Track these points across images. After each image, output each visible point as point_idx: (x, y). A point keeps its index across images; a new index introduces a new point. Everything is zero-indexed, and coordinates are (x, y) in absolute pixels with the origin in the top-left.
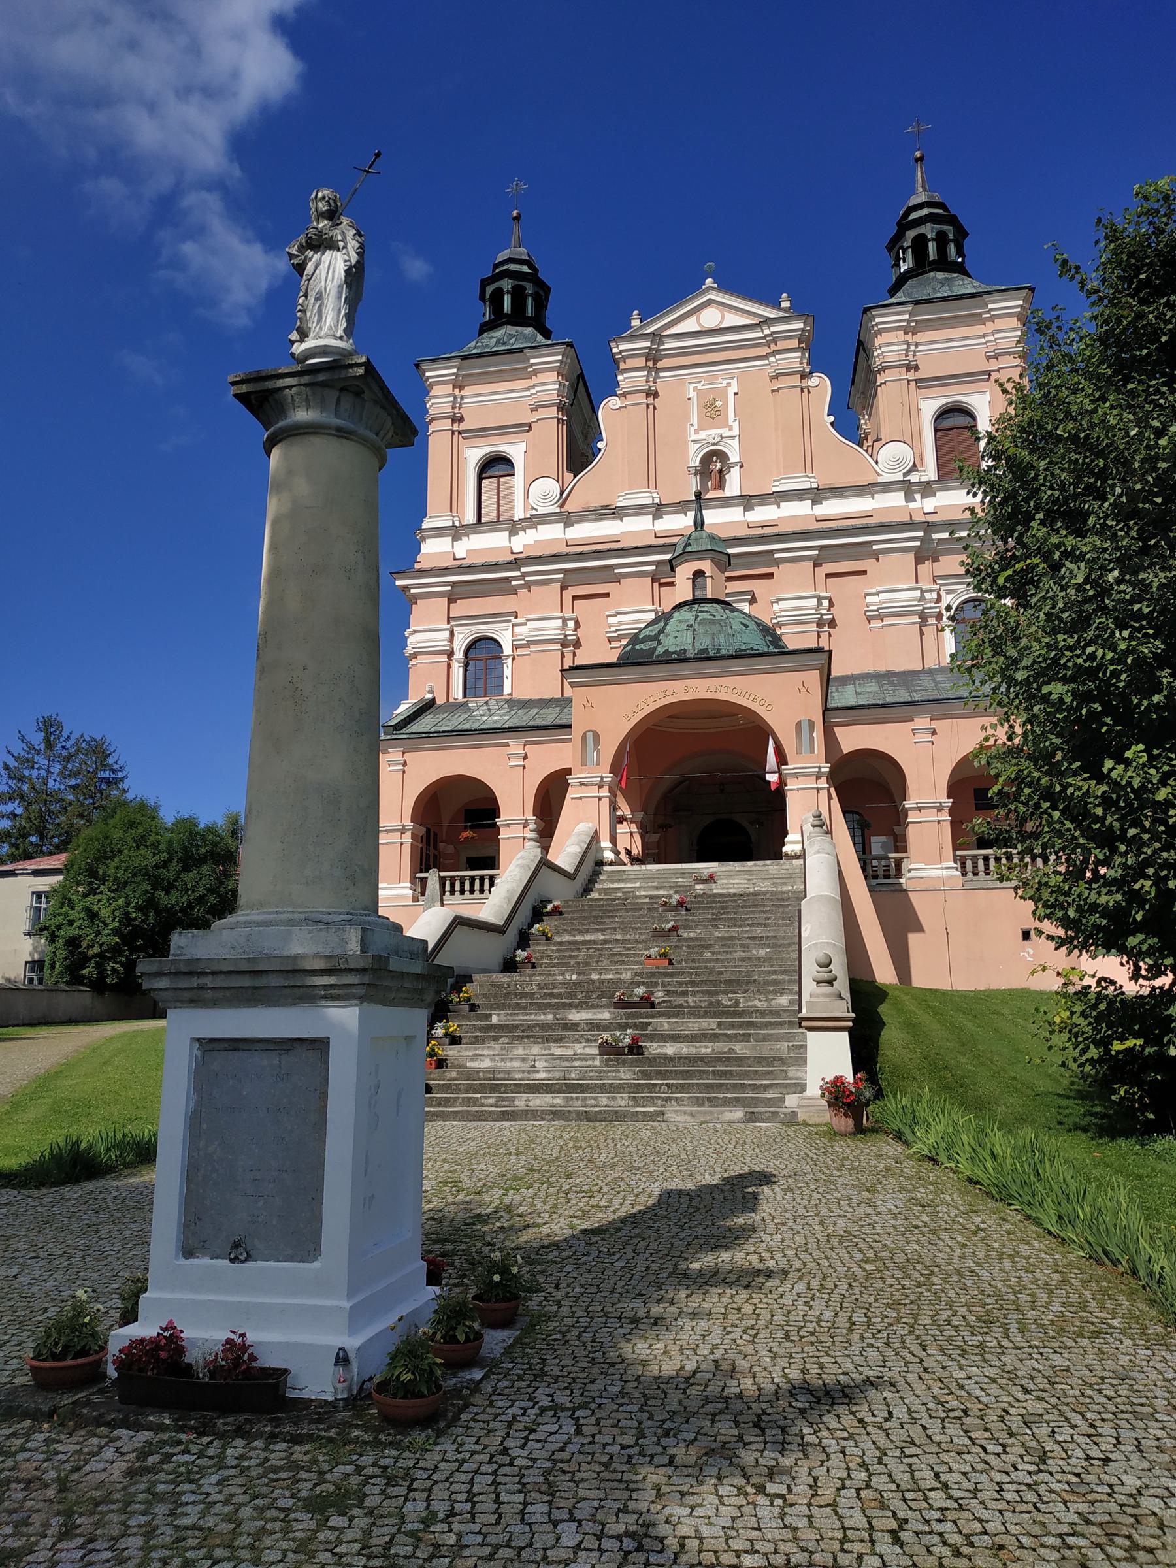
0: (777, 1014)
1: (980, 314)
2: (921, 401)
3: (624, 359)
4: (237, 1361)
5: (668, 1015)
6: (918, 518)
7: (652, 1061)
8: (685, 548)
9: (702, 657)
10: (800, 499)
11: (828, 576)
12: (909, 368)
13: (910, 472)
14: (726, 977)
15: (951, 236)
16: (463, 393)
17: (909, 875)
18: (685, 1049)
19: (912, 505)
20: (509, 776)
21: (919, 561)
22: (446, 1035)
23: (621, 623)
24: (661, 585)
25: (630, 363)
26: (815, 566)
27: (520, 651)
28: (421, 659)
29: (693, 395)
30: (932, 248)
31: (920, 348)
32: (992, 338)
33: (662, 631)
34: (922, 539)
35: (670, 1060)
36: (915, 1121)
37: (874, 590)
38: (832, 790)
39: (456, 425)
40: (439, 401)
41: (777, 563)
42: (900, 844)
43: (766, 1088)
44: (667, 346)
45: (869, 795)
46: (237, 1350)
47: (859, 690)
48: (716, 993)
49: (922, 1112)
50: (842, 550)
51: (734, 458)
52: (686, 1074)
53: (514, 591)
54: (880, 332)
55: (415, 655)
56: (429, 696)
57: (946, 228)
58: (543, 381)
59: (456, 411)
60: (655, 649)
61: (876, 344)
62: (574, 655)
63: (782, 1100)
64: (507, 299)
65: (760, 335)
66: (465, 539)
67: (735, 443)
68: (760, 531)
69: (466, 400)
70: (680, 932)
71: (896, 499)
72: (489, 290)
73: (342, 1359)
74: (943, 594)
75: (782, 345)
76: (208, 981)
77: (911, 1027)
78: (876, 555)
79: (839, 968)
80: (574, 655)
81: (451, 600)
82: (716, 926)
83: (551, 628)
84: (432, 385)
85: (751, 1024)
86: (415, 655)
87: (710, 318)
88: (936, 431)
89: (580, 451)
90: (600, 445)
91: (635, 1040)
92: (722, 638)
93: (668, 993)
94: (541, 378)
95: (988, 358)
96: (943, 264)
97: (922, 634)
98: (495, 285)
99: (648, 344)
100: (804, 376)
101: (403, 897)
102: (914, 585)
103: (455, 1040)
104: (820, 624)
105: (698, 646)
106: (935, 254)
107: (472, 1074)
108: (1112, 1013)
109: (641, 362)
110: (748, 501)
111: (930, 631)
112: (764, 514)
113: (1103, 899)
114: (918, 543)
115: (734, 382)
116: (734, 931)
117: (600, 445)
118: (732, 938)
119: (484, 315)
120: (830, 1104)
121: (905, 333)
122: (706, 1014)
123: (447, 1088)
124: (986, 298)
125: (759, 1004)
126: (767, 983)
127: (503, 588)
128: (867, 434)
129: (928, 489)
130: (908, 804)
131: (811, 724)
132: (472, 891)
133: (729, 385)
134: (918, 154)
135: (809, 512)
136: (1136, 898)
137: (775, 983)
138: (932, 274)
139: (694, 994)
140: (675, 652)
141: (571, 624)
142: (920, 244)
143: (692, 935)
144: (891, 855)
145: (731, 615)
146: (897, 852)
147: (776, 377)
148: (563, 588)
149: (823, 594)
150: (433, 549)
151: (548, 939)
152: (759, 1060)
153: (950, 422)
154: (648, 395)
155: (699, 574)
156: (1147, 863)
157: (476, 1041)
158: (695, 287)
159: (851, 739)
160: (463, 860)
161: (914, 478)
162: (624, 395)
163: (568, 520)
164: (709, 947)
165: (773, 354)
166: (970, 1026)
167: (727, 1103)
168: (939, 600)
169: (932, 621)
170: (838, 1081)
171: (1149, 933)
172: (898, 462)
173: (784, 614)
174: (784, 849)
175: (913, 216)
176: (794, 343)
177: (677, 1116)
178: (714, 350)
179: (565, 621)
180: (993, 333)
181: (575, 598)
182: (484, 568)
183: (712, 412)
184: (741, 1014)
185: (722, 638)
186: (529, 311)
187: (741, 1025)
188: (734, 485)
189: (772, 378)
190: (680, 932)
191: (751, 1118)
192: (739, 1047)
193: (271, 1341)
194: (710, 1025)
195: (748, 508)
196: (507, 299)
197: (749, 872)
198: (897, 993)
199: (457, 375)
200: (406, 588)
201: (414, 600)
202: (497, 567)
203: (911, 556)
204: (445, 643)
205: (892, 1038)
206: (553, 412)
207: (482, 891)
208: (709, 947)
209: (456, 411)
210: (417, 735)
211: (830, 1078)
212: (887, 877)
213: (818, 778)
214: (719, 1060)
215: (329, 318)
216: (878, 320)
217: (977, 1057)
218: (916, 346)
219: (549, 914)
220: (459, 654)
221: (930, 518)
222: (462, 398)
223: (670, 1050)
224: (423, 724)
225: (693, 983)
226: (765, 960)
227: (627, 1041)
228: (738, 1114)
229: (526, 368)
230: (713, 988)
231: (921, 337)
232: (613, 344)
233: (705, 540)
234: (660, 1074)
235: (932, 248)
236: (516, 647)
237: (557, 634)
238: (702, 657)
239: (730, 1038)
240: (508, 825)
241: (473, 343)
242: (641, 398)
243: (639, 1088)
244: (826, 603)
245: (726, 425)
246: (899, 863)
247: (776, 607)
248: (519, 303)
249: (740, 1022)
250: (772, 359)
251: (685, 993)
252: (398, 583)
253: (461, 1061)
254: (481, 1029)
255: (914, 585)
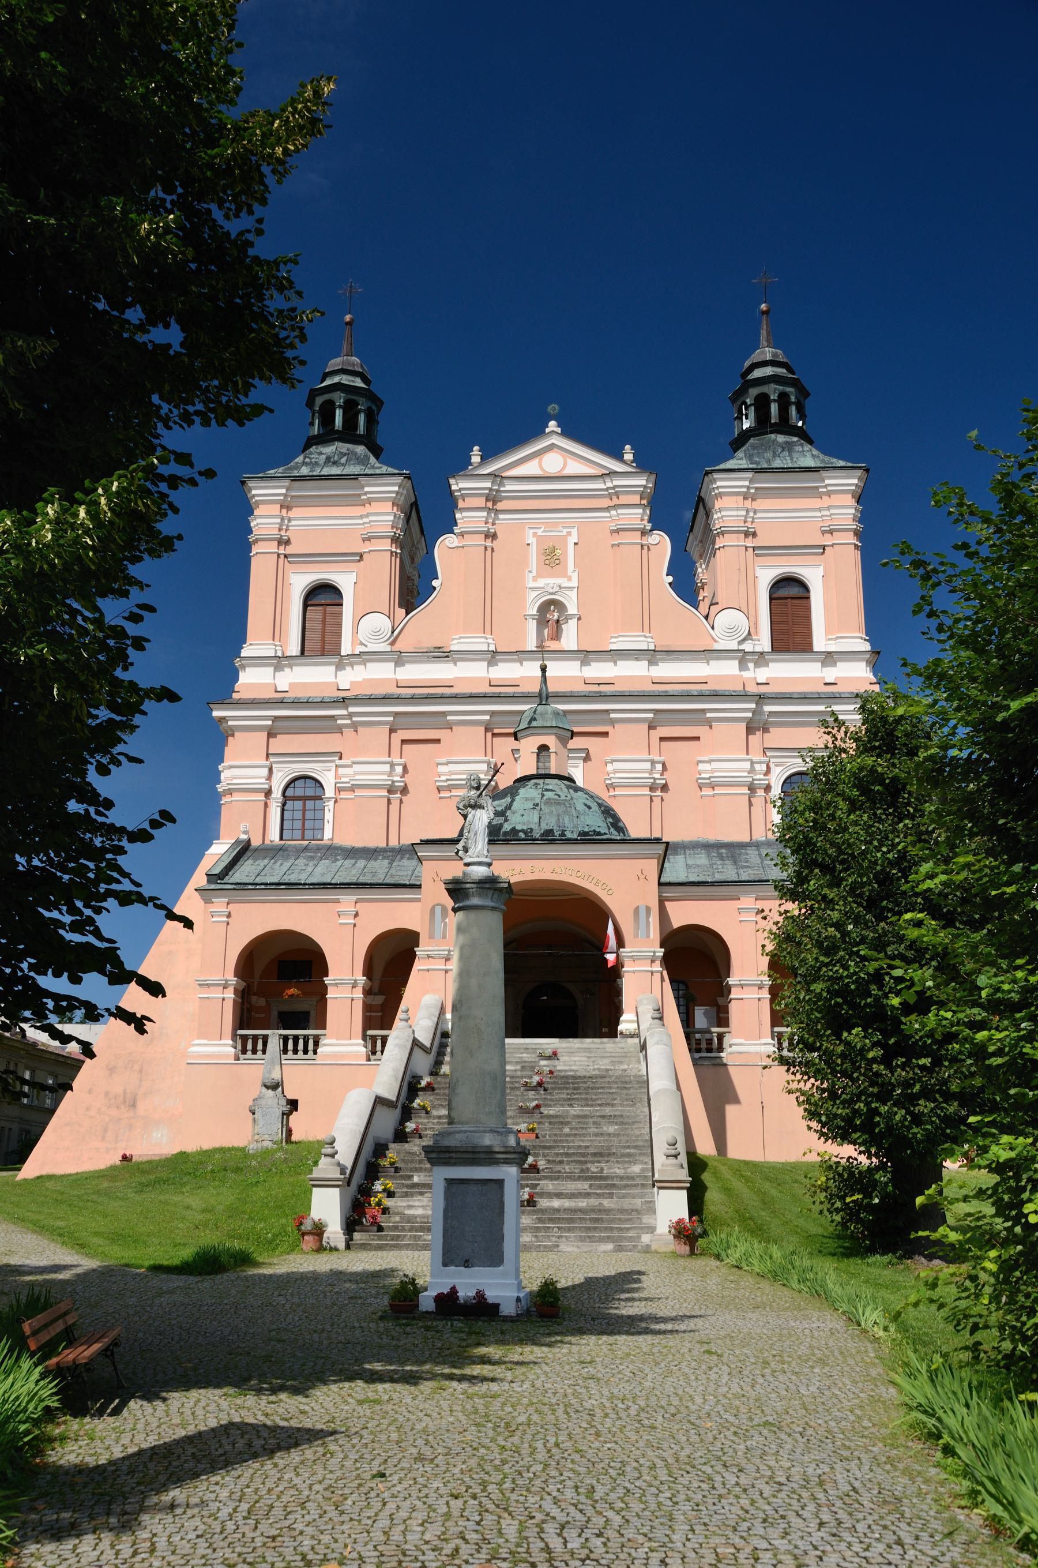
0: (632, 1178)
1: (817, 488)
2: (757, 569)
3: (463, 497)
4: (479, 1302)
5: (551, 1179)
6: (752, 689)
7: (543, 1211)
8: (530, 722)
9: (548, 838)
10: (637, 659)
11: (662, 739)
12: (747, 534)
13: (744, 640)
14: (592, 1151)
15: (793, 399)
16: (291, 514)
17: (729, 1050)
18: (567, 1203)
19: (746, 674)
20: (343, 934)
21: (750, 730)
22: (384, 1190)
23: (451, 773)
24: (494, 735)
25: (469, 502)
26: (650, 728)
27: (343, 795)
28: (237, 797)
29: (532, 540)
30: (774, 408)
31: (759, 515)
32: (827, 513)
33: (509, 807)
34: (754, 712)
35: (558, 1210)
36: (728, 1247)
37: (706, 758)
38: (665, 973)
39: (282, 548)
40: (264, 522)
41: (613, 722)
42: (722, 1018)
43: (628, 1229)
44: (508, 488)
45: (696, 965)
46: (480, 1295)
47: (690, 862)
48: (586, 1162)
49: (733, 1240)
50: (679, 714)
51: (572, 609)
52: (571, 1220)
53: (339, 730)
54: (720, 495)
55: (230, 792)
56: (244, 837)
57: (788, 389)
58: (376, 508)
59: (283, 533)
60: (501, 825)
61: (717, 507)
62: (401, 801)
63: (640, 1237)
64: (339, 413)
65: (602, 486)
66: (287, 670)
67: (573, 594)
68: (596, 688)
69: (293, 523)
70: (545, 1111)
71: (729, 668)
72: (319, 401)
73: (518, 1299)
74: (772, 766)
75: (624, 500)
76: (453, 1155)
77: (727, 1191)
78: (709, 723)
79: (681, 1147)
80: (401, 801)
81: (271, 735)
82: (571, 1105)
83: (378, 773)
84: (258, 503)
85: (613, 1186)
86: (230, 792)
87: (552, 463)
88: (771, 599)
89: (414, 587)
90: (435, 583)
91: (531, 1196)
92: (567, 820)
93: (549, 1161)
94: (375, 507)
95: (823, 533)
96: (784, 427)
97: (751, 804)
98: (327, 397)
99: (489, 485)
100: (644, 533)
101: (357, 1056)
102: (745, 756)
103: (390, 1194)
104: (652, 789)
105: (544, 827)
106: (781, 417)
107: (410, 1219)
108: (848, 1179)
109: (481, 502)
110: (585, 656)
111: (758, 802)
112: (600, 670)
113: (840, 1111)
114: (750, 715)
115: (574, 532)
116: (587, 1110)
117: (435, 583)
118: (585, 1116)
119: (312, 424)
120: (675, 1237)
121: (745, 499)
122: (579, 1178)
123: (395, 1228)
124: (824, 474)
125: (618, 1170)
126: (623, 1155)
127: (329, 726)
128: (704, 584)
129: (761, 659)
130: (731, 981)
131: (648, 910)
132: (306, 1052)
133: (569, 534)
134: (763, 307)
135: (645, 673)
136: (856, 1112)
137: (630, 1155)
138: (773, 436)
139: (568, 1163)
140: (522, 831)
141: (399, 770)
142: (762, 404)
143: (552, 1112)
144: (714, 1029)
145: (575, 795)
146: (719, 1026)
147: (617, 531)
148: (392, 731)
149: (657, 758)
150: (251, 680)
151: (427, 1112)
152: (622, 1211)
153: (783, 592)
154: (487, 537)
155: (543, 748)
156: (861, 1093)
157: (406, 1195)
158: (537, 431)
159: (684, 913)
160: (275, 1014)
161: (748, 647)
162: (462, 534)
163: (399, 659)
164: (568, 1123)
165: (615, 507)
166: (774, 1192)
167: (602, 1240)
168: (768, 771)
169: (761, 793)
170: (680, 1221)
171: (864, 1132)
172: (733, 630)
173: (618, 775)
174: (620, 1028)
175: (758, 373)
176: (636, 499)
177: (566, 1247)
178: (555, 496)
179: (392, 765)
180: (829, 508)
181: (403, 742)
182: (308, 703)
183: (551, 558)
184: (606, 1178)
185: (567, 820)
186: (361, 429)
187: (606, 1187)
188: (570, 638)
189: (613, 532)
190: (542, 1110)
191: (619, 1249)
192: (606, 1203)
193: (492, 1295)
194: (583, 1186)
195: (585, 662)
196: (339, 413)
197: (588, 1050)
198: (715, 1164)
199: (285, 495)
200: (223, 719)
201: (231, 732)
202: (322, 703)
203: (743, 726)
204: (263, 781)
205: (713, 1197)
206: (386, 545)
207: (306, 1051)
208: (568, 1123)
209: (283, 533)
210: (242, 886)
211: (675, 1219)
212: (709, 1050)
213: (653, 961)
214: (593, 1211)
215: (480, 846)
216: (719, 484)
217: (774, 1212)
218: (755, 512)
219: (423, 1089)
220: (277, 794)
221: (763, 689)
222: (289, 520)
223: (556, 1203)
224: (245, 872)
225: (567, 1155)
226: (614, 1136)
227: (526, 1197)
228: (610, 1246)
229: (359, 495)
230: (582, 1157)
231: (760, 504)
232: (452, 481)
233: (550, 716)
234: (551, 1220)
235: (774, 408)
236: (339, 790)
237: (384, 779)
238: (548, 838)
239: (599, 1195)
240: (336, 985)
241: (300, 459)
242: (480, 540)
243: (538, 1229)
244: (659, 767)
245: (564, 574)
246: (721, 1037)
247: (610, 768)
248: (350, 422)
249: (605, 1184)
250: (613, 512)
251: (561, 1162)
252: (216, 714)
253: (400, 1210)
254: (407, 1186)
255: (745, 756)
